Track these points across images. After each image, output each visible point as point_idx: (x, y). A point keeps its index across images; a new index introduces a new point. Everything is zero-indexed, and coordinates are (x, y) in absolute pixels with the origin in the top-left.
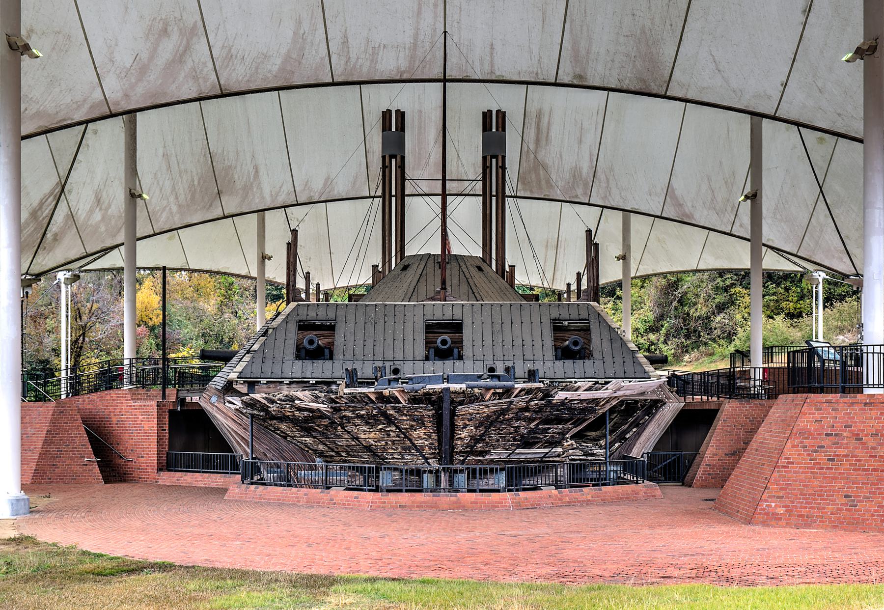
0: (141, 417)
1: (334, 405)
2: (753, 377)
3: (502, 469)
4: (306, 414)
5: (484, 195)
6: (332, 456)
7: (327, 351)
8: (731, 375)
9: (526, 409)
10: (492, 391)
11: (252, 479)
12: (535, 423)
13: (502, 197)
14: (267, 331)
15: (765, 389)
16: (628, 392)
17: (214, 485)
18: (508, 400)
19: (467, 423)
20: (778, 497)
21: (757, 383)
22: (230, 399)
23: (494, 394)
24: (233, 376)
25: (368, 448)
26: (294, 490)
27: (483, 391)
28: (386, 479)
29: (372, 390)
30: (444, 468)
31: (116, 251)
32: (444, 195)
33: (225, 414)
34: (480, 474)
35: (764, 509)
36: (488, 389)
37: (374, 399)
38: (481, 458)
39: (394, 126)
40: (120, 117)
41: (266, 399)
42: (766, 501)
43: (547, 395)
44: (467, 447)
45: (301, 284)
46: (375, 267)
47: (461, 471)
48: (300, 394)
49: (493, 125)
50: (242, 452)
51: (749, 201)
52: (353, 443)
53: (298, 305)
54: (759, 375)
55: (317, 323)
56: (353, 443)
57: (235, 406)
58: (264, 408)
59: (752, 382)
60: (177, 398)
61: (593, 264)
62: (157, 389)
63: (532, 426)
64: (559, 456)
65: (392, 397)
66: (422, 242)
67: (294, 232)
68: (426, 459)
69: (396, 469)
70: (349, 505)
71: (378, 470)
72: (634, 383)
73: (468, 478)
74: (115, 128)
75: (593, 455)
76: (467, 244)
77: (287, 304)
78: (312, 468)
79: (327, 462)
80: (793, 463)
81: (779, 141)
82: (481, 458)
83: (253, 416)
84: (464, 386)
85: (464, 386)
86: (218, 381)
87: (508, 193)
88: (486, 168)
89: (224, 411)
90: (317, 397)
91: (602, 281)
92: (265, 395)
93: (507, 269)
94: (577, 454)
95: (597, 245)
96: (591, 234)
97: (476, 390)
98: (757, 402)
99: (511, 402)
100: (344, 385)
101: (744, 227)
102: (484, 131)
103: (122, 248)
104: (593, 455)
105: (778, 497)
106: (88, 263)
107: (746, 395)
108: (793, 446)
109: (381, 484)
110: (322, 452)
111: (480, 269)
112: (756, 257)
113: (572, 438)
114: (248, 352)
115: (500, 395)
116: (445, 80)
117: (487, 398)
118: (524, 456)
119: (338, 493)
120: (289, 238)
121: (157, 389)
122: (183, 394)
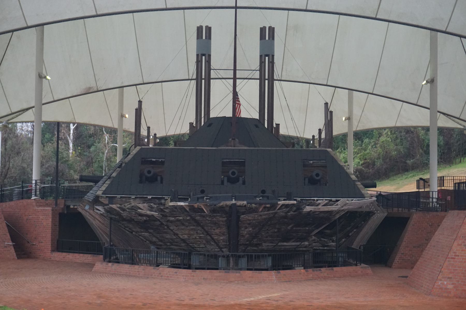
0: (41, 217)
1: (163, 213)
2: (431, 196)
3: (269, 256)
4: (145, 218)
5: (260, 79)
6: (161, 245)
7: (159, 178)
8: (416, 195)
9: (285, 217)
10: (264, 206)
11: (110, 258)
12: (290, 226)
13: (208, 79)
14: (121, 164)
15: (439, 204)
16: (351, 207)
17: (87, 261)
18: (274, 211)
19: (247, 226)
20: (449, 278)
21: (435, 200)
22: (97, 207)
23: (265, 207)
24: (100, 193)
25: (184, 241)
26: (136, 267)
27: (257, 206)
28: (195, 260)
29: (187, 204)
30: (232, 255)
31: (31, 110)
32: (235, 79)
33: (95, 216)
34: (255, 258)
35: (439, 285)
36: (261, 204)
37: (188, 210)
38: (256, 248)
39: (204, 35)
40: (34, 28)
41: (119, 208)
42: (441, 280)
43: (298, 208)
44: (247, 241)
45: (144, 132)
46: (191, 124)
47: (243, 256)
48: (141, 206)
49: (267, 35)
50: (105, 239)
51: (429, 84)
52: (175, 237)
53: (141, 149)
54: (435, 195)
55: (153, 160)
56: (175, 237)
57: (100, 212)
58: (119, 214)
59: (431, 200)
60: (65, 205)
61: (329, 124)
62: (51, 200)
63: (289, 227)
64: (305, 247)
65: (199, 209)
66: (221, 108)
67: (140, 102)
68: (221, 248)
69: (201, 254)
70: (171, 277)
71: (190, 254)
72: (355, 201)
73: (248, 261)
74: (32, 33)
75: (327, 246)
76: (249, 110)
77: (135, 147)
78: (148, 252)
79: (158, 248)
80: (458, 256)
81: (449, 47)
82: (256, 248)
83: (111, 219)
84: (245, 203)
85: (245, 203)
86: (90, 196)
87: (275, 78)
88: (262, 63)
89: (94, 215)
90: (152, 207)
91: (335, 133)
92: (119, 206)
93: (275, 126)
94: (317, 246)
95: (331, 112)
96: (327, 106)
97: (253, 205)
98: (435, 213)
99: (276, 213)
100: (169, 200)
101: (426, 101)
102: (260, 40)
103: (33, 109)
104: (327, 246)
105: (449, 278)
106: (13, 118)
107: (427, 209)
108: (459, 245)
109: (192, 263)
110: (155, 242)
111: (257, 126)
112: (433, 119)
113: (314, 235)
114: (109, 178)
115: (269, 209)
116: (236, 8)
117: (261, 210)
118: (283, 247)
119: (166, 270)
120: (137, 106)
121: (51, 200)
122: (68, 203)
